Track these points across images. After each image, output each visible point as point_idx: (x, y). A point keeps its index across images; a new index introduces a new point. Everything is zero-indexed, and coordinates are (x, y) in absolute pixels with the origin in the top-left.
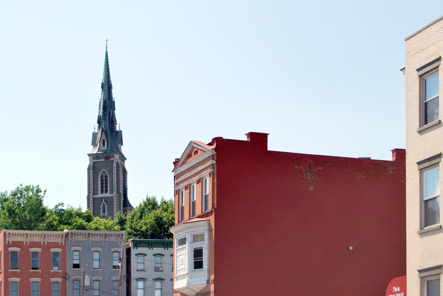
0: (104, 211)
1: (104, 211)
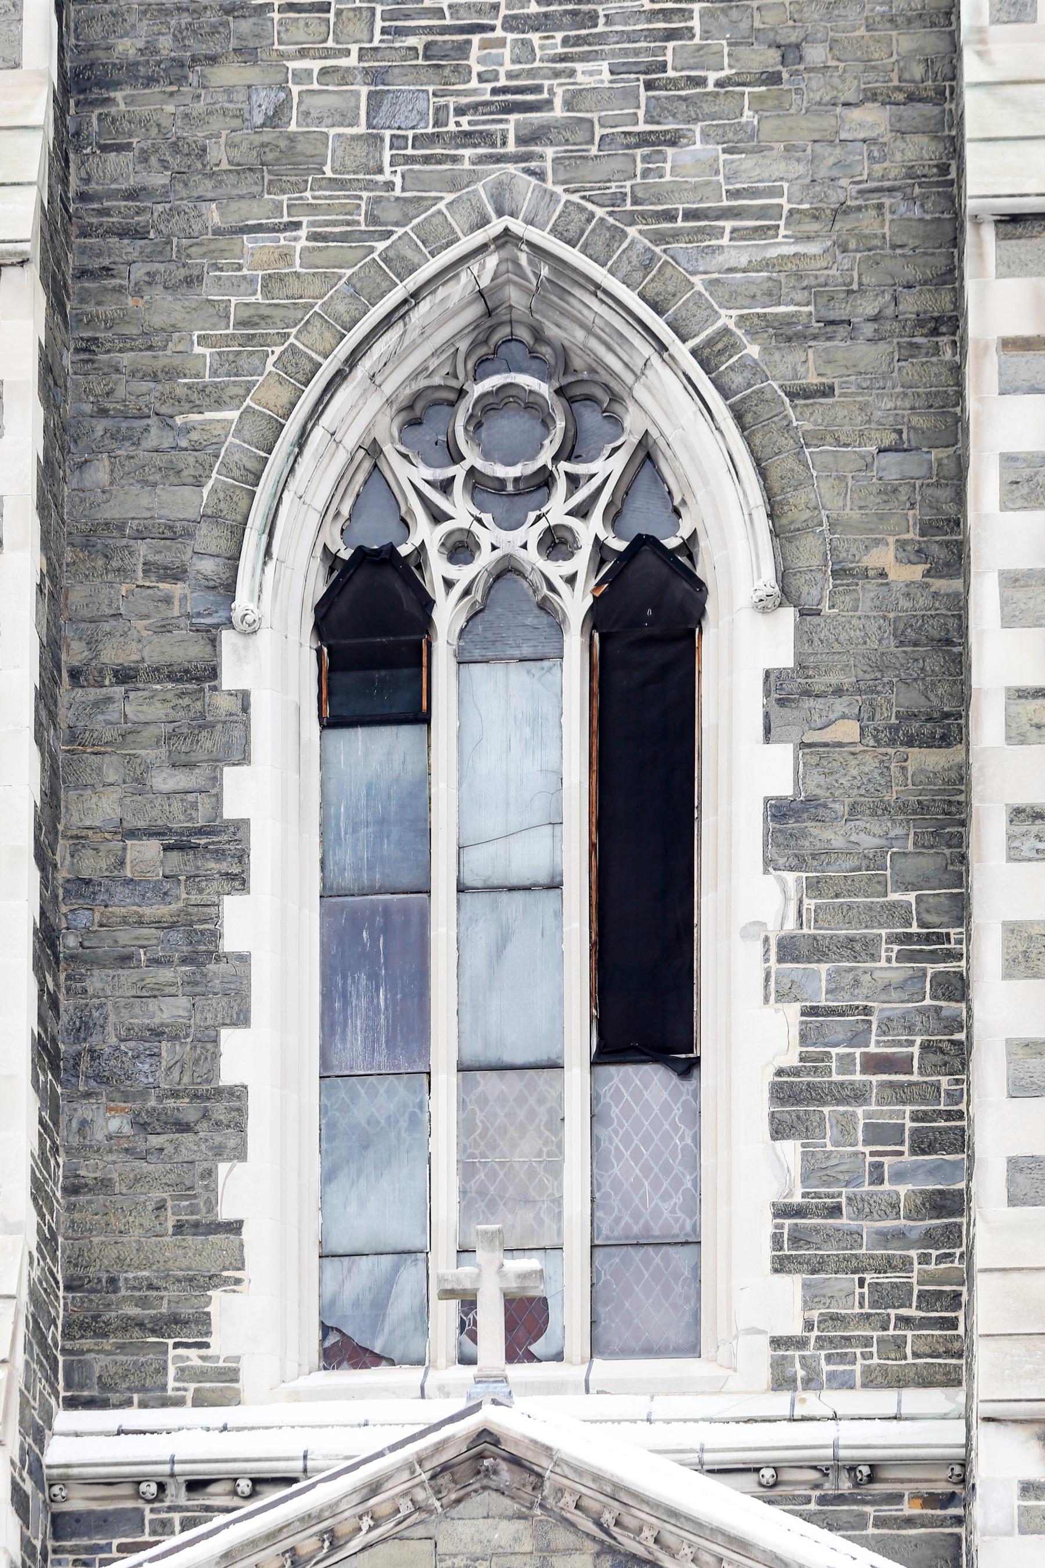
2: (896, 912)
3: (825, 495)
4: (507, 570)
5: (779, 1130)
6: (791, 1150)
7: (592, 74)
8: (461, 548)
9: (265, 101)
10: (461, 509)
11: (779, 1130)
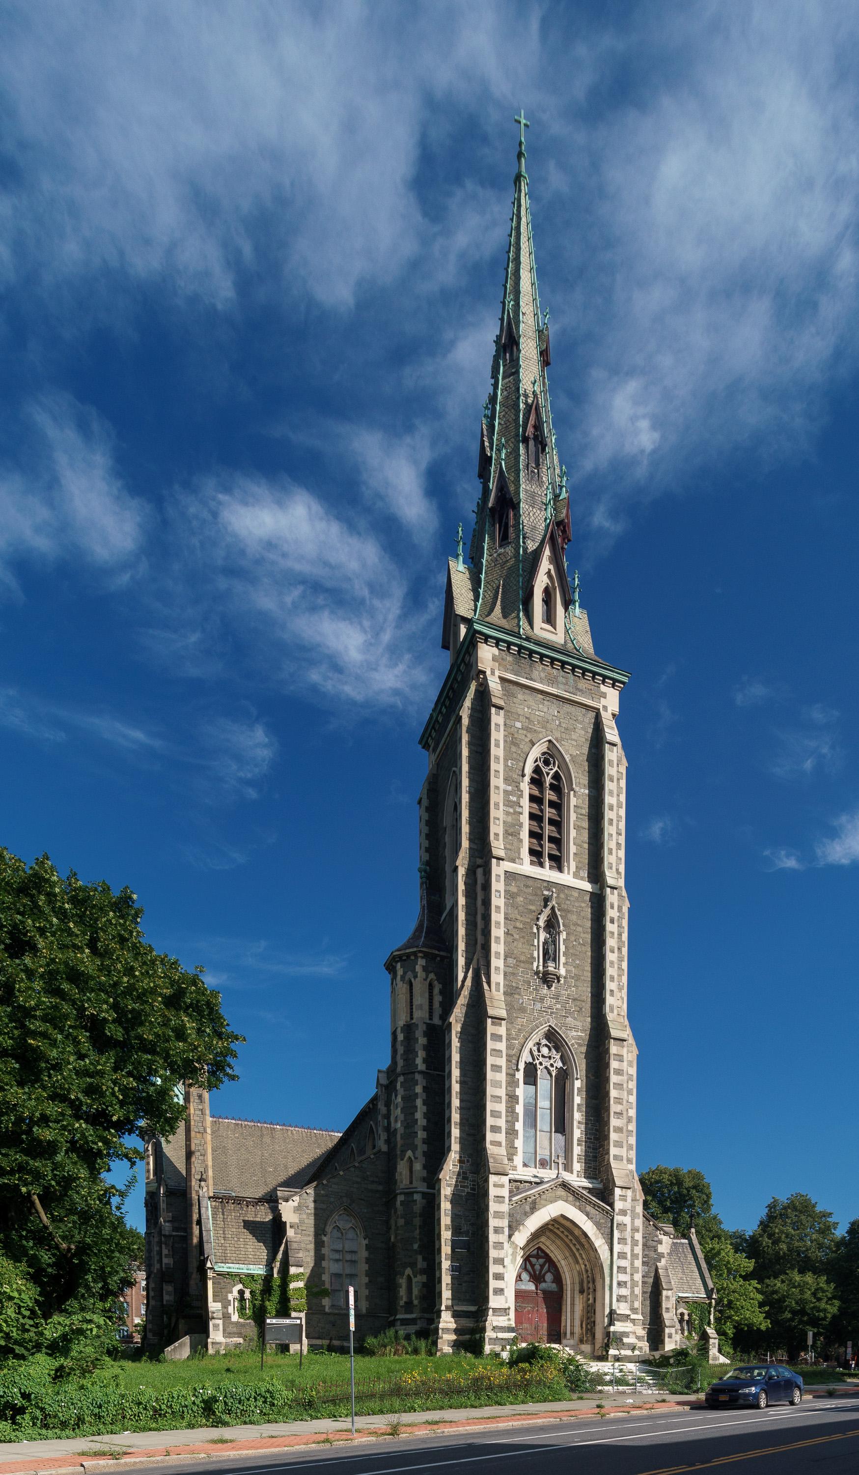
7: (559, 1006)
8: (541, 1064)
9: (521, 1001)
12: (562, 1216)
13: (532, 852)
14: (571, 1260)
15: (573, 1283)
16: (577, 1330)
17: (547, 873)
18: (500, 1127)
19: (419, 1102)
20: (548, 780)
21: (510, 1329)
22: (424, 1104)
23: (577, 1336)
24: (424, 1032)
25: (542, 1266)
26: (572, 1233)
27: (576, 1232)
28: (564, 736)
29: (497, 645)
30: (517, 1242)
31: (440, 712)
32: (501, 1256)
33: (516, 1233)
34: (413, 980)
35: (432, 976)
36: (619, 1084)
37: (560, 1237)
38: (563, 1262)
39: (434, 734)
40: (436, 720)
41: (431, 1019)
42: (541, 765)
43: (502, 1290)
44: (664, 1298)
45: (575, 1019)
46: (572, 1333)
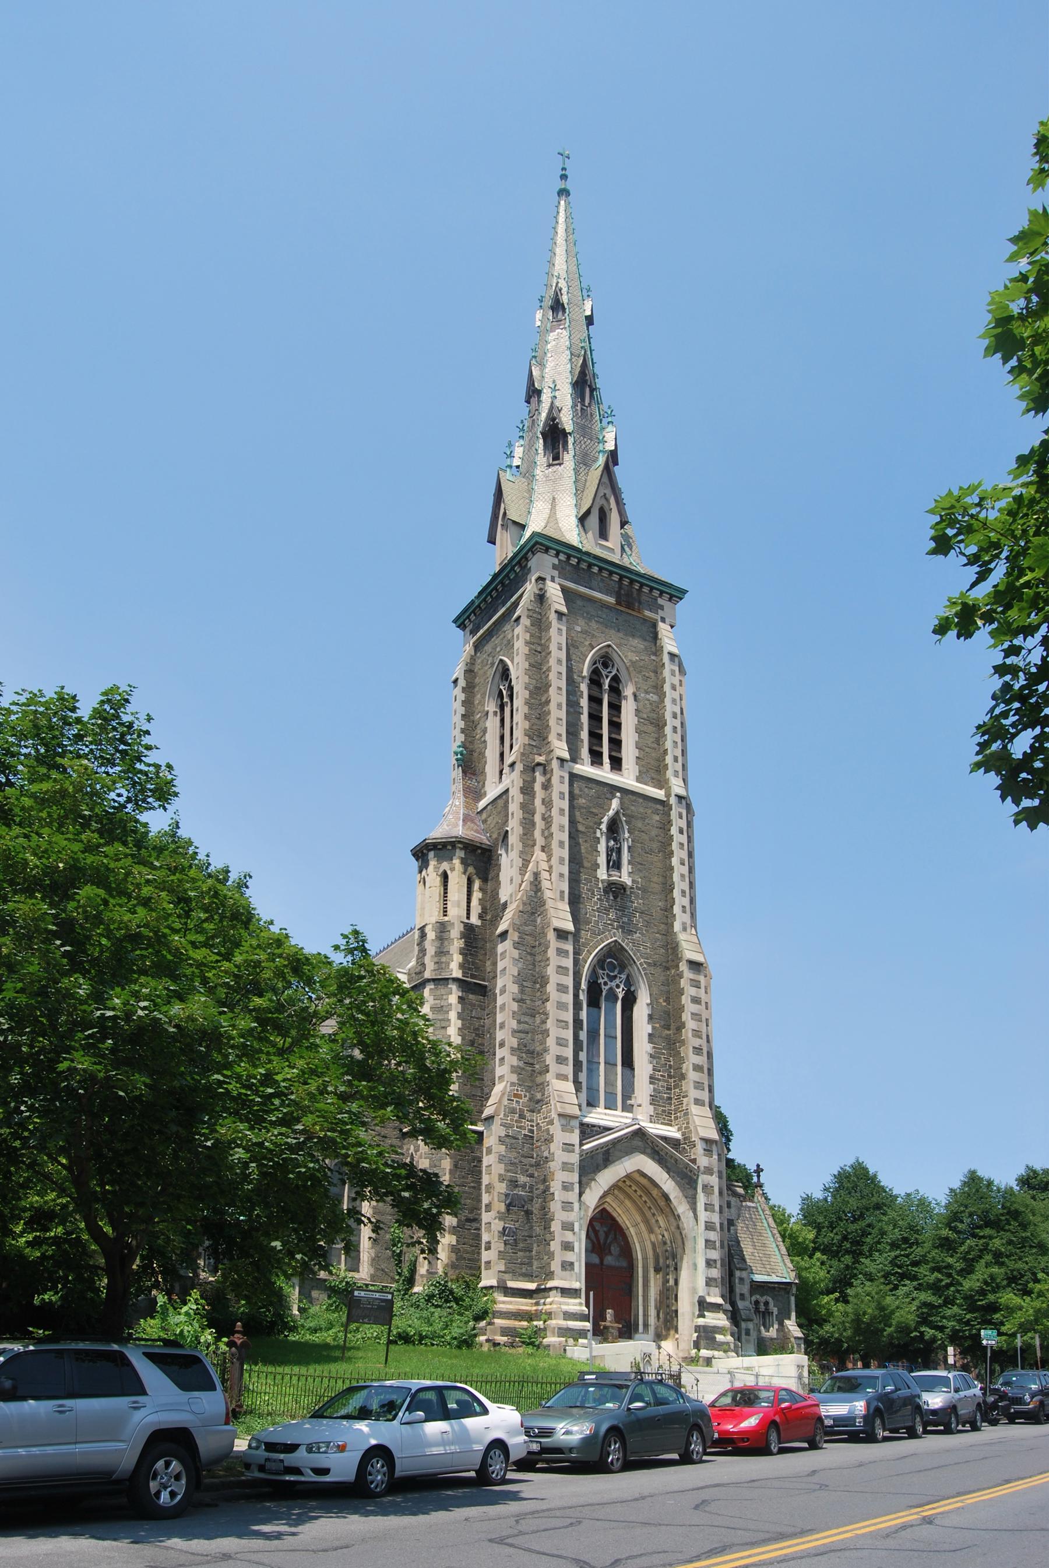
0: (615, 865)
1: (615, 865)
2: (663, 1054)
3: (655, 991)
4: (611, 989)
5: (651, 1083)
6: (652, 1086)
10: (606, 979)
11: (651, 1083)
12: (639, 1171)
13: (592, 752)
14: (642, 1226)
15: (645, 1259)
16: (652, 1320)
17: (604, 773)
18: (567, 1059)
19: (453, 1015)
20: (606, 683)
21: (584, 1318)
22: (459, 1018)
23: (652, 1330)
24: (461, 933)
25: (607, 1234)
26: (648, 1193)
27: (655, 1192)
28: (623, 641)
29: (557, 555)
30: (588, 1203)
31: (484, 600)
32: (570, 1219)
33: (588, 1191)
34: (449, 872)
35: (471, 869)
36: (696, 1014)
37: (630, 1197)
38: (632, 1230)
39: (473, 617)
40: (479, 606)
41: (468, 918)
42: (600, 667)
43: (572, 1264)
44: (737, 1281)
45: (642, 934)
46: (646, 1325)
